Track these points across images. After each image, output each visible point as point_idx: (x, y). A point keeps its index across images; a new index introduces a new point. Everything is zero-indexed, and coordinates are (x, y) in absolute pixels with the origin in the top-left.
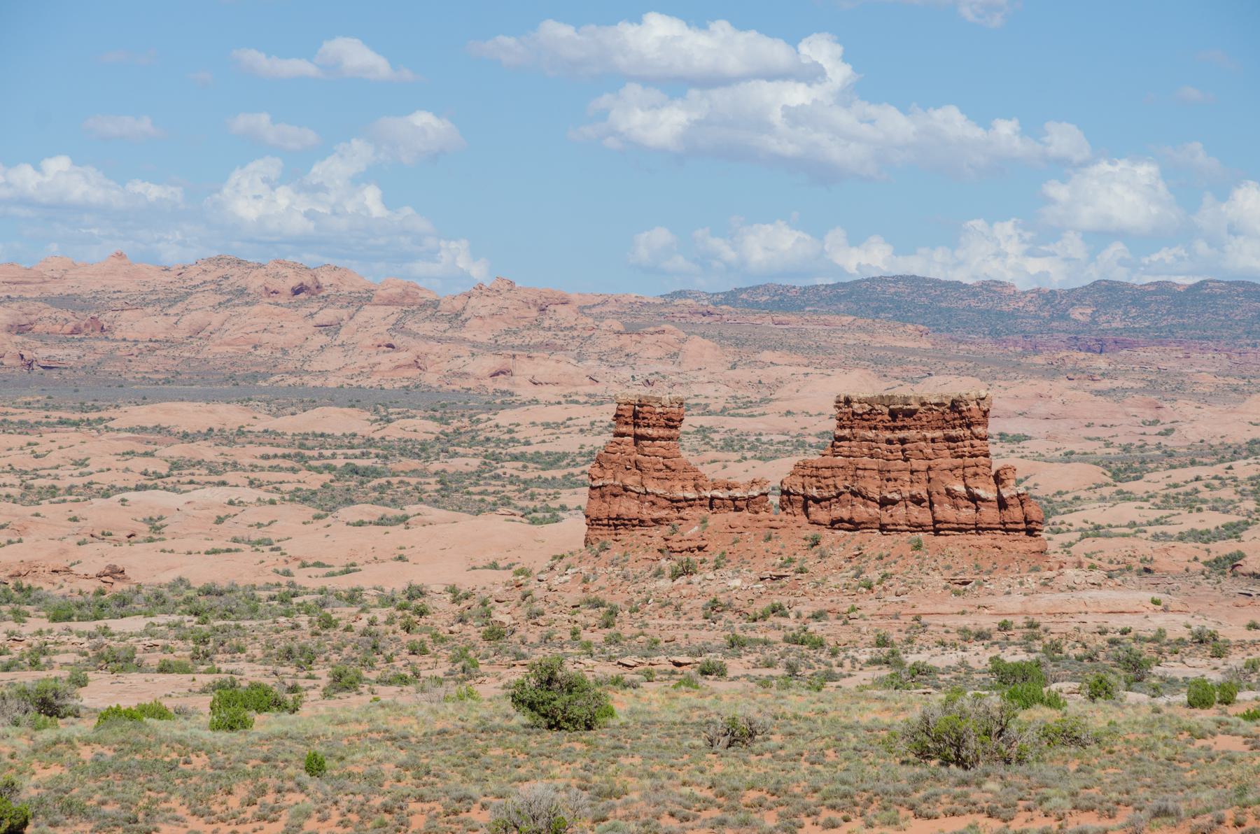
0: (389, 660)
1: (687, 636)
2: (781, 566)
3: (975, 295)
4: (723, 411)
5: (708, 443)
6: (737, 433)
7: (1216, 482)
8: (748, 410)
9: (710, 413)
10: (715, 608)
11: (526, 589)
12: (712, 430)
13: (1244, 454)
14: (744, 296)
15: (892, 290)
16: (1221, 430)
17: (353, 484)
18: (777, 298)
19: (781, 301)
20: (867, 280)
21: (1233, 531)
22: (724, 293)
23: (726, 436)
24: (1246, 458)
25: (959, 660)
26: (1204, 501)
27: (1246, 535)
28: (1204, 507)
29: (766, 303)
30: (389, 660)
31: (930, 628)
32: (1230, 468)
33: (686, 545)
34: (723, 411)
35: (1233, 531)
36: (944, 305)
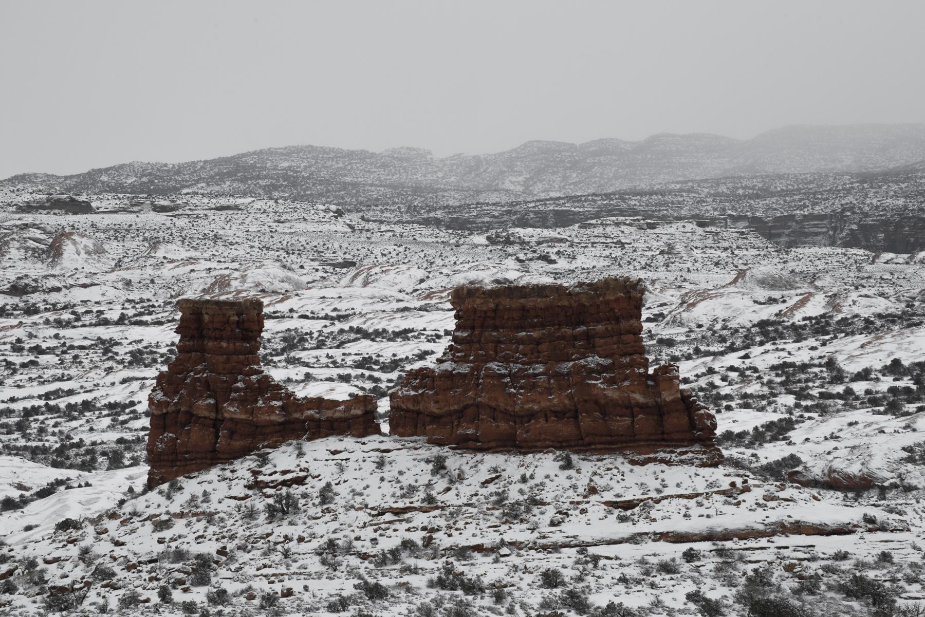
0: (745, 574)
1: (306, 588)
2: (403, 496)
3: (384, 166)
4: (121, 321)
5: (112, 358)
6: (145, 344)
7: (734, 375)
8: (154, 317)
9: (106, 322)
10: (330, 552)
11: (83, 544)
12: (113, 343)
13: (758, 339)
14: (105, 178)
15: (286, 164)
16: (108, 330)
17: (779, 380)
18: (145, 179)
19: (151, 182)
20: (254, 153)
21: (778, 431)
22: (78, 176)
23: (130, 348)
24: (762, 344)
25: (653, 598)
26: (728, 397)
27: (796, 435)
28: (733, 404)
29: (132, 186)
30: (745, 574)
31: (602, 562)
32: (746, 356)
33: (279, 478)
34: (121, 321)
35: (778, 431)
36: (348, 179)
